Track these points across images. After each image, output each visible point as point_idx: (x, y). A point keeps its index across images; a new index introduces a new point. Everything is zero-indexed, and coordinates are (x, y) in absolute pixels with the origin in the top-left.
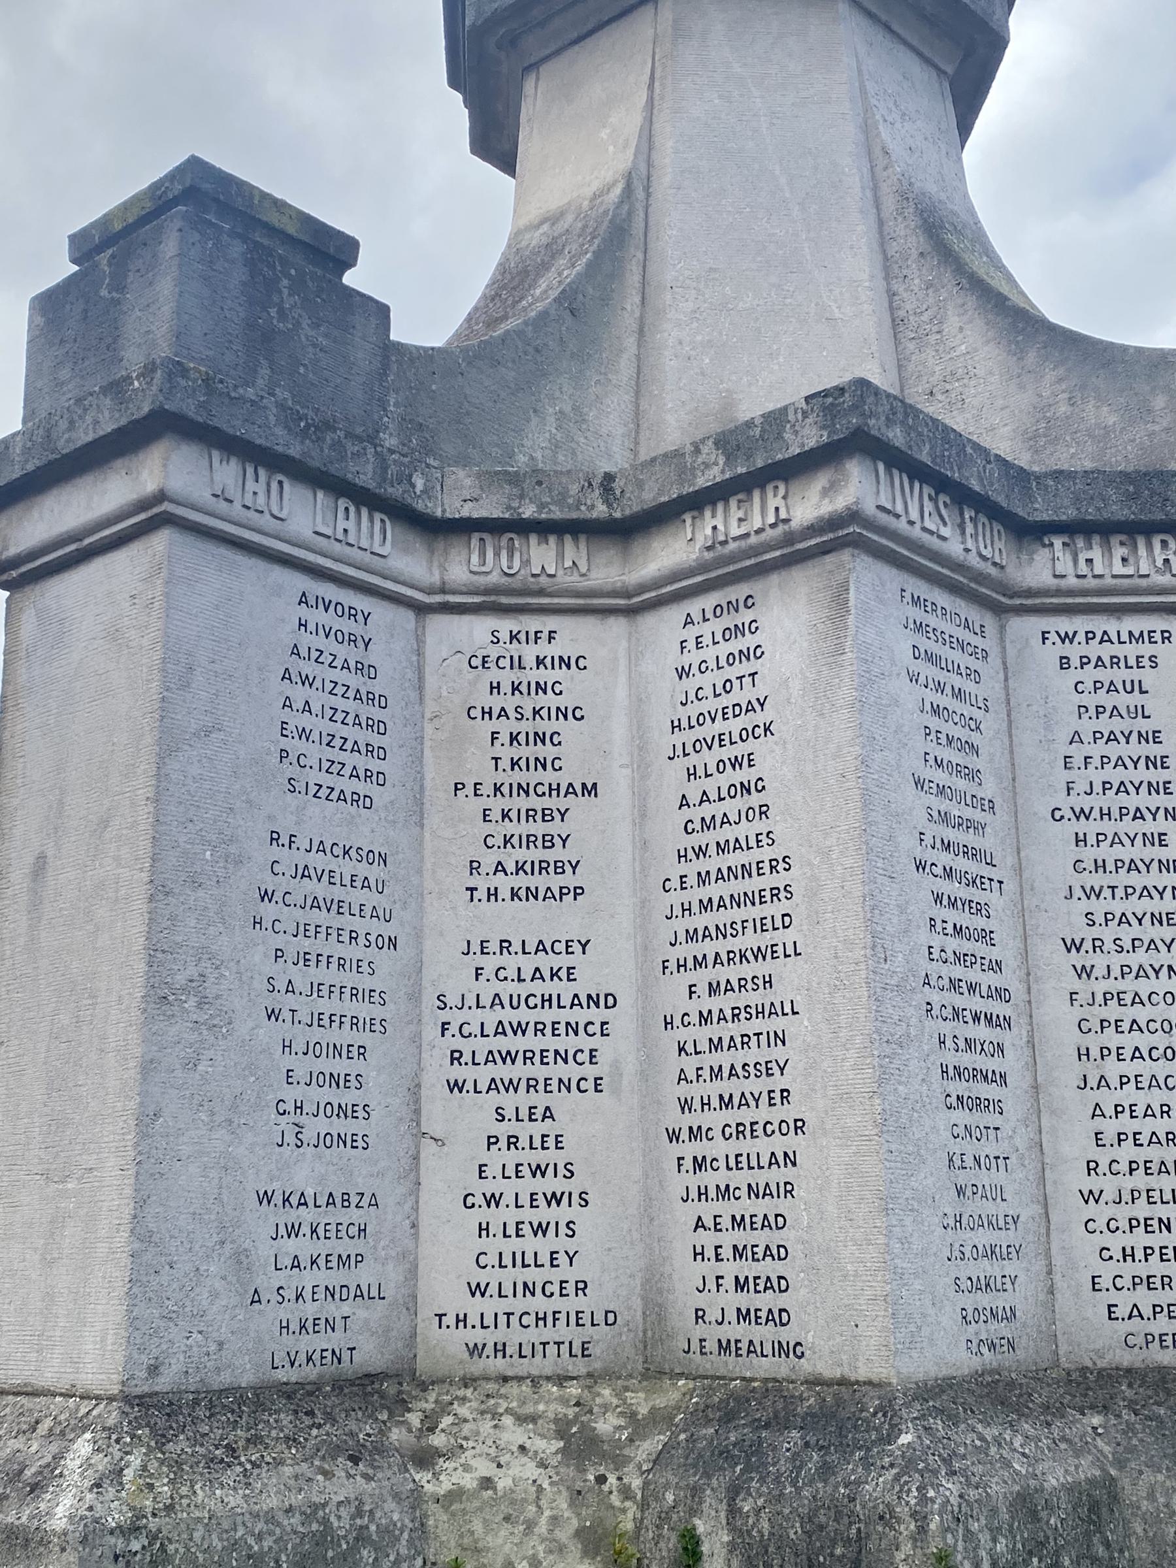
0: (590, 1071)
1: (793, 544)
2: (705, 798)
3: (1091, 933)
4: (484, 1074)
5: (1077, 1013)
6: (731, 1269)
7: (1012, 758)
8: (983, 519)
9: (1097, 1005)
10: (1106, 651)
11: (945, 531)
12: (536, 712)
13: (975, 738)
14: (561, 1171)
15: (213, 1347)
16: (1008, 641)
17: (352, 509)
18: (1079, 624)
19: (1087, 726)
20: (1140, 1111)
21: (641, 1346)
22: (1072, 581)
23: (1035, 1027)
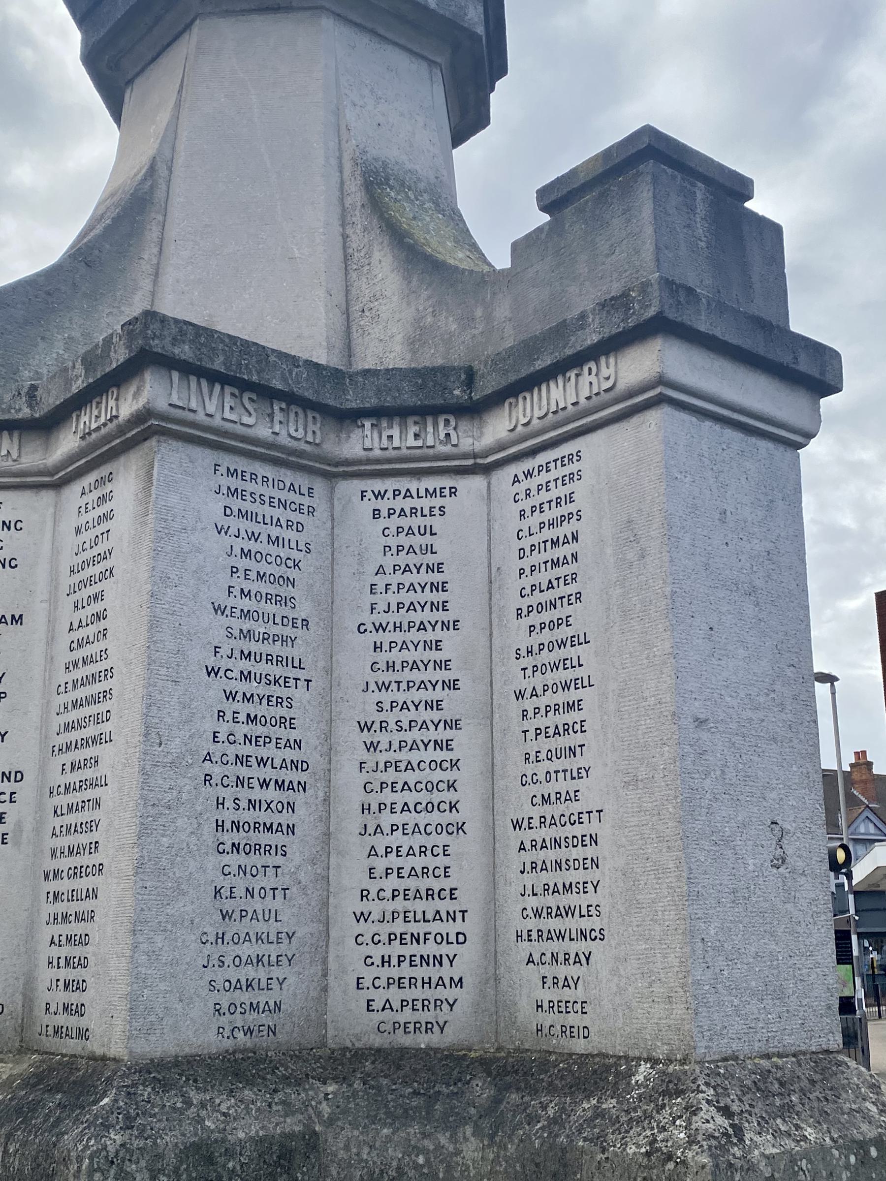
1: (125, 434)
3: (378, 717)
5: (364, 777)
7: (332, 587)
9: (379, 771)
10: (408, 504)
11: (246, 420)
13: (292, 574)
16: (335, 500)
18: (390, 484)
19: (389, 562)
20: (404, 851)
21: (20, 1030)
22: (377, 453)
23: (332, 789)
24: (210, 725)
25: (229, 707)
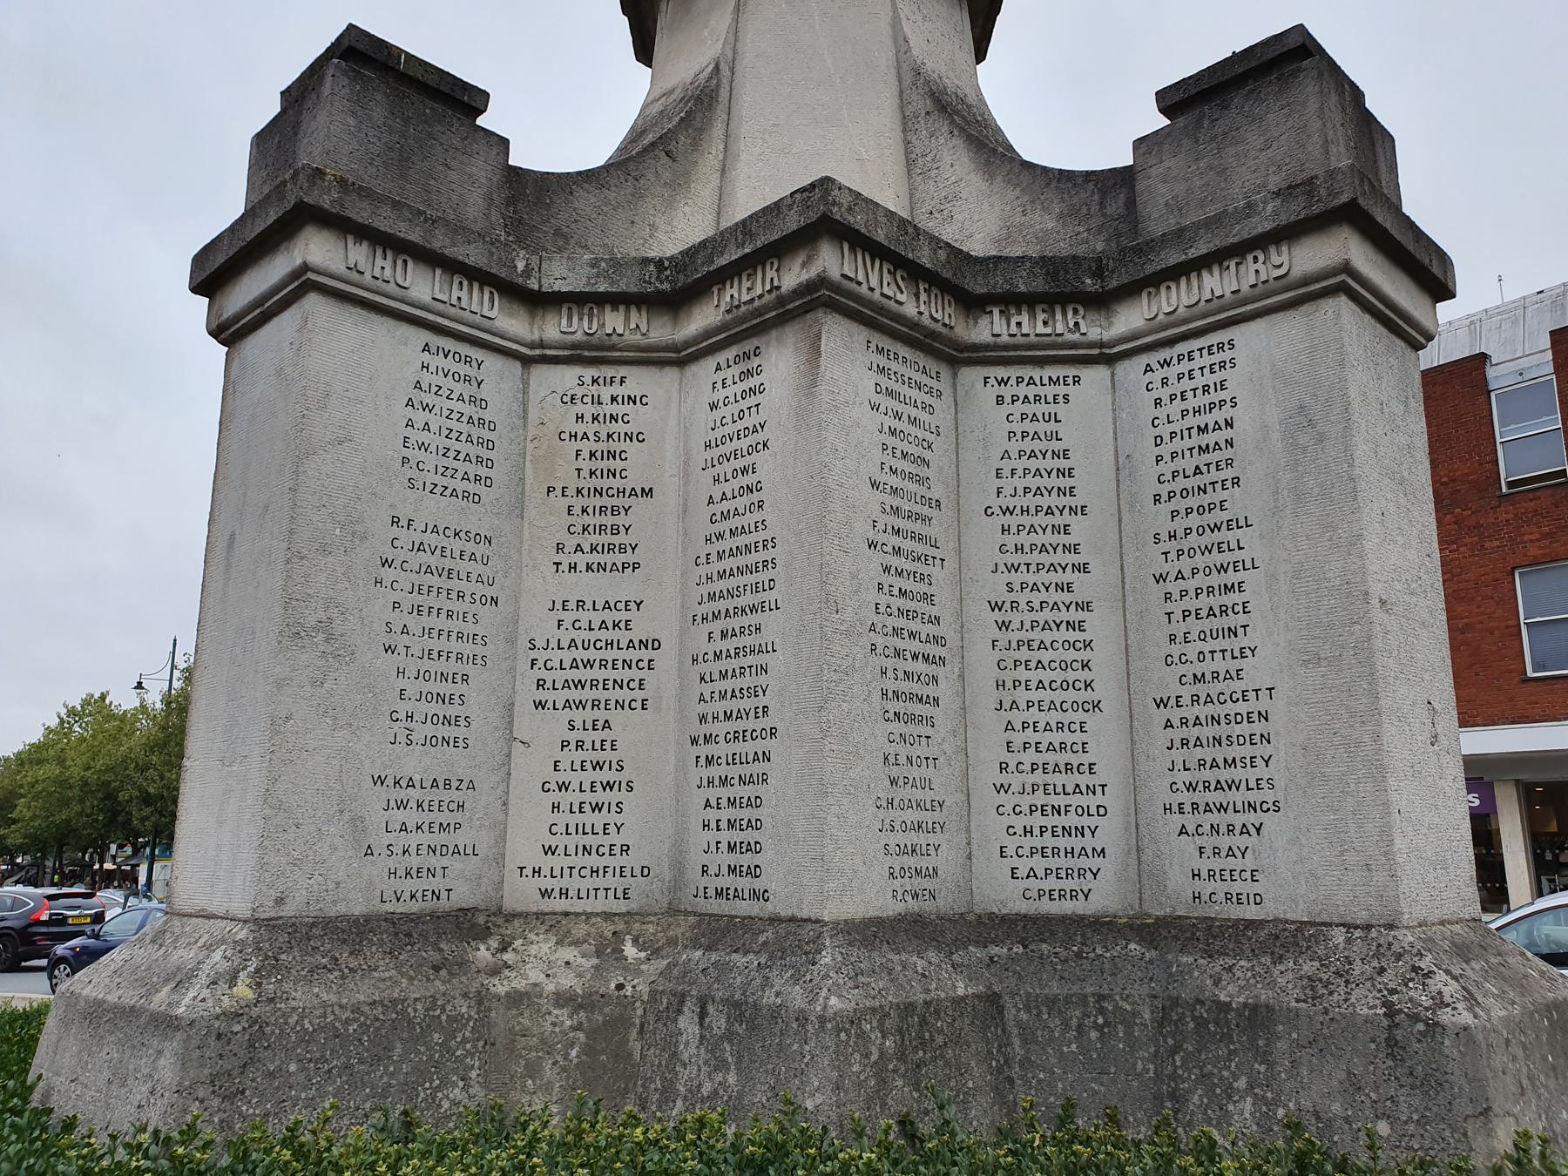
0: (638, 695)
2: (724, 497)
4: (561, 696)
5: (997, 655)
6: (726, 836)
8: (935, 291)
11: (901, 298)
12: (609, 436)
13: (927, 455)
14: (614, 766)
15: (332, 886)
17: (465, 283)
18: (1012, 372)
19: (1014, 446)
20: (1041, 726)
22: (1005, 338)
24: (872, 596)
25: (887, 580)
